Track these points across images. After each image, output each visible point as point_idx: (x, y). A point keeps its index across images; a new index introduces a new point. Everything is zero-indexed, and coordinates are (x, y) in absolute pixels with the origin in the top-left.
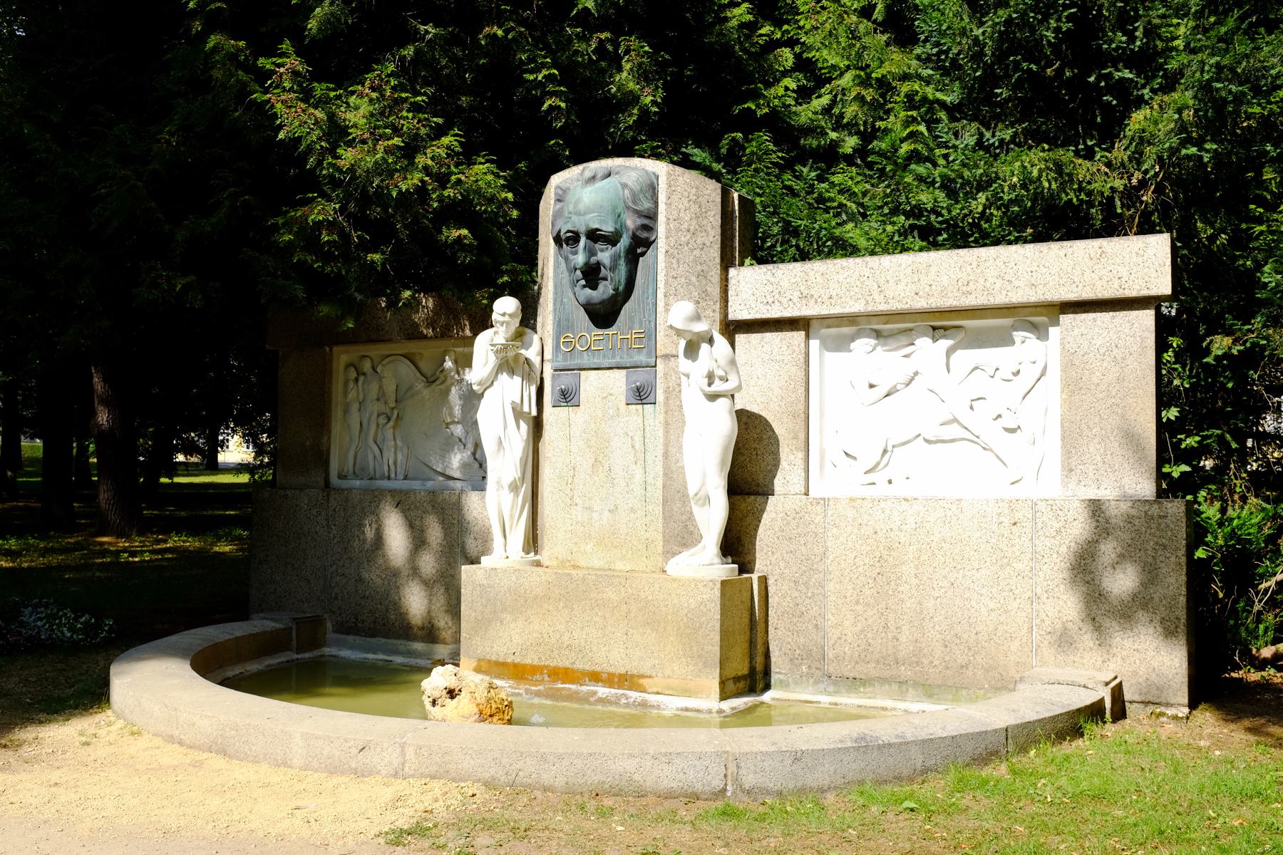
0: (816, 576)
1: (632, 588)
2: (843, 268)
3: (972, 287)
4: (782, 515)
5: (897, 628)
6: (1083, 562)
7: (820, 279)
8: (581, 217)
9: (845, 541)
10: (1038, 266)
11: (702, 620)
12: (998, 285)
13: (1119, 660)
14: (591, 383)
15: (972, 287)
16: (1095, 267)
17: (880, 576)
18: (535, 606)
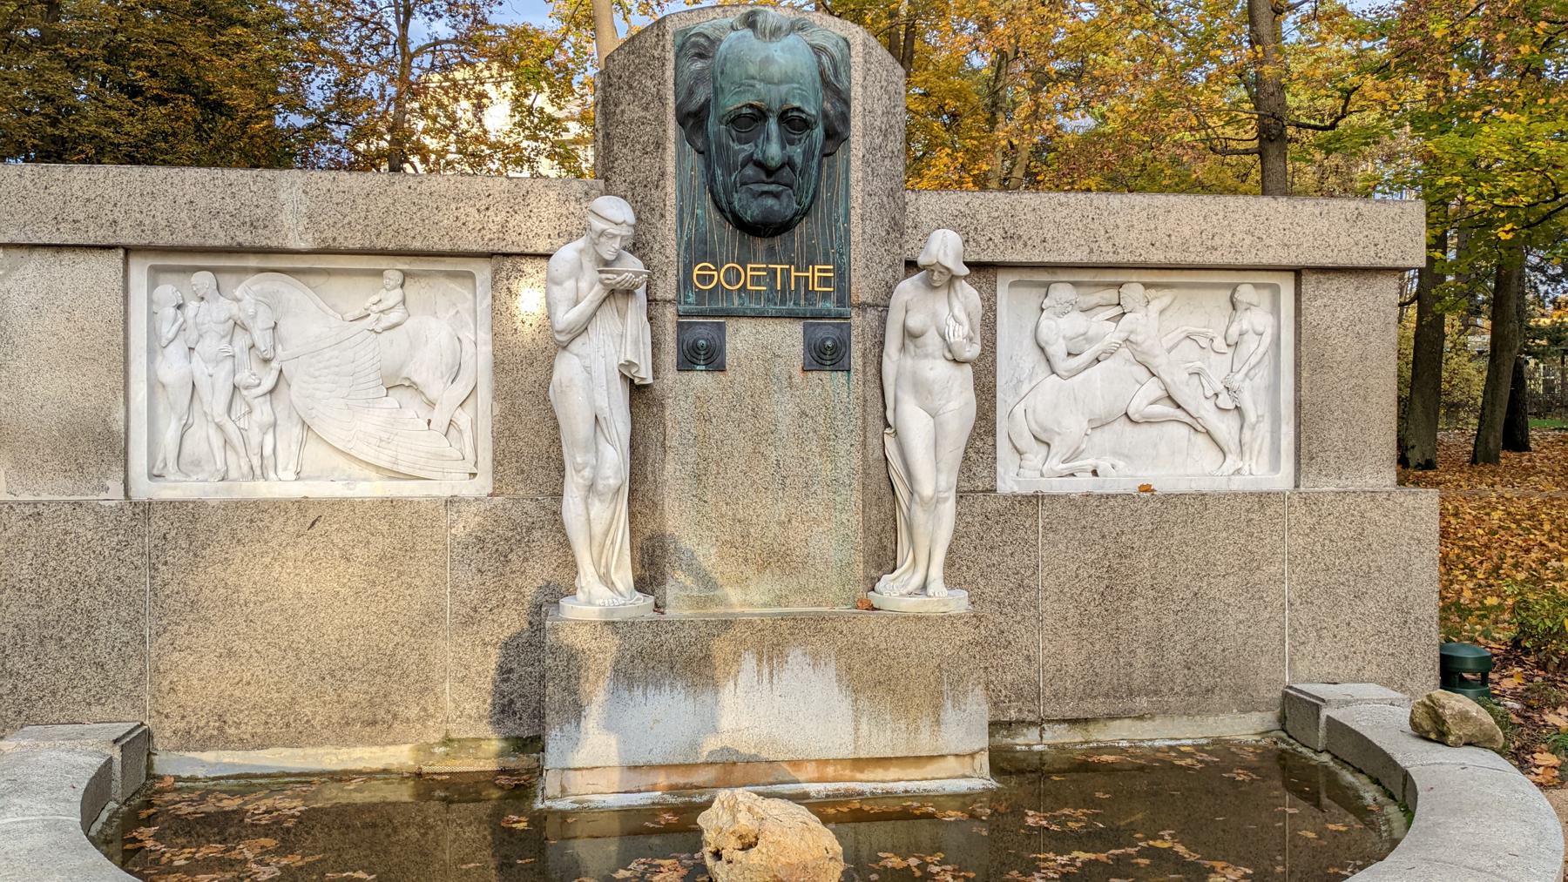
0: (1027, 595)
1: (853, 634)
2: (1061, 205)
3: (1217, 242)
4: (980, 518)
5: (1130, 653)
6: (1338, 561)
7: (1030, 216)
8: (773, 87)
9: (1064, 549)
10: (1291, 224)
11: (963, 671)
12: (1248, 242)
13: (1375, 667)
14: (741, 338)
15: (1217, 242)
16: (1351, 230)
17: (1109, 589)
18: (689, 674)
